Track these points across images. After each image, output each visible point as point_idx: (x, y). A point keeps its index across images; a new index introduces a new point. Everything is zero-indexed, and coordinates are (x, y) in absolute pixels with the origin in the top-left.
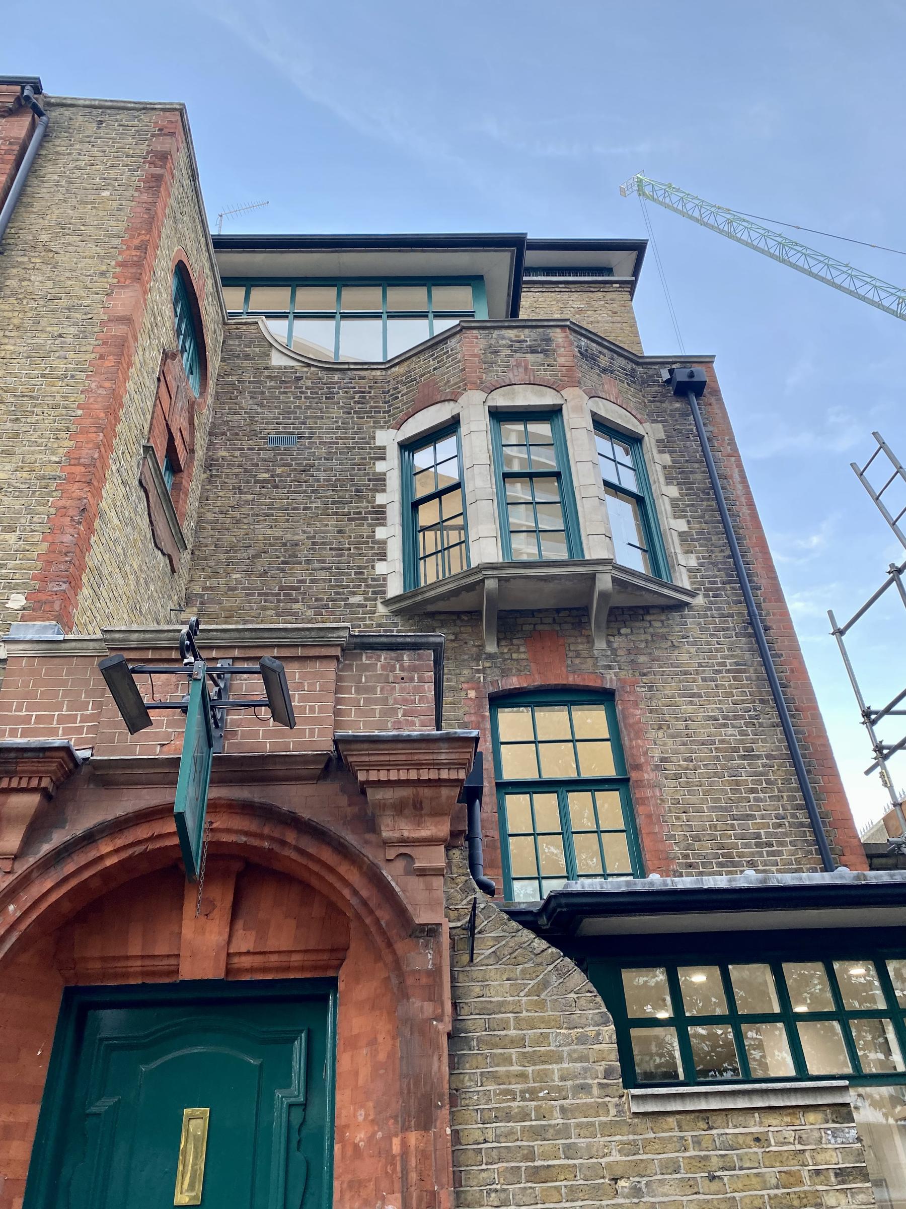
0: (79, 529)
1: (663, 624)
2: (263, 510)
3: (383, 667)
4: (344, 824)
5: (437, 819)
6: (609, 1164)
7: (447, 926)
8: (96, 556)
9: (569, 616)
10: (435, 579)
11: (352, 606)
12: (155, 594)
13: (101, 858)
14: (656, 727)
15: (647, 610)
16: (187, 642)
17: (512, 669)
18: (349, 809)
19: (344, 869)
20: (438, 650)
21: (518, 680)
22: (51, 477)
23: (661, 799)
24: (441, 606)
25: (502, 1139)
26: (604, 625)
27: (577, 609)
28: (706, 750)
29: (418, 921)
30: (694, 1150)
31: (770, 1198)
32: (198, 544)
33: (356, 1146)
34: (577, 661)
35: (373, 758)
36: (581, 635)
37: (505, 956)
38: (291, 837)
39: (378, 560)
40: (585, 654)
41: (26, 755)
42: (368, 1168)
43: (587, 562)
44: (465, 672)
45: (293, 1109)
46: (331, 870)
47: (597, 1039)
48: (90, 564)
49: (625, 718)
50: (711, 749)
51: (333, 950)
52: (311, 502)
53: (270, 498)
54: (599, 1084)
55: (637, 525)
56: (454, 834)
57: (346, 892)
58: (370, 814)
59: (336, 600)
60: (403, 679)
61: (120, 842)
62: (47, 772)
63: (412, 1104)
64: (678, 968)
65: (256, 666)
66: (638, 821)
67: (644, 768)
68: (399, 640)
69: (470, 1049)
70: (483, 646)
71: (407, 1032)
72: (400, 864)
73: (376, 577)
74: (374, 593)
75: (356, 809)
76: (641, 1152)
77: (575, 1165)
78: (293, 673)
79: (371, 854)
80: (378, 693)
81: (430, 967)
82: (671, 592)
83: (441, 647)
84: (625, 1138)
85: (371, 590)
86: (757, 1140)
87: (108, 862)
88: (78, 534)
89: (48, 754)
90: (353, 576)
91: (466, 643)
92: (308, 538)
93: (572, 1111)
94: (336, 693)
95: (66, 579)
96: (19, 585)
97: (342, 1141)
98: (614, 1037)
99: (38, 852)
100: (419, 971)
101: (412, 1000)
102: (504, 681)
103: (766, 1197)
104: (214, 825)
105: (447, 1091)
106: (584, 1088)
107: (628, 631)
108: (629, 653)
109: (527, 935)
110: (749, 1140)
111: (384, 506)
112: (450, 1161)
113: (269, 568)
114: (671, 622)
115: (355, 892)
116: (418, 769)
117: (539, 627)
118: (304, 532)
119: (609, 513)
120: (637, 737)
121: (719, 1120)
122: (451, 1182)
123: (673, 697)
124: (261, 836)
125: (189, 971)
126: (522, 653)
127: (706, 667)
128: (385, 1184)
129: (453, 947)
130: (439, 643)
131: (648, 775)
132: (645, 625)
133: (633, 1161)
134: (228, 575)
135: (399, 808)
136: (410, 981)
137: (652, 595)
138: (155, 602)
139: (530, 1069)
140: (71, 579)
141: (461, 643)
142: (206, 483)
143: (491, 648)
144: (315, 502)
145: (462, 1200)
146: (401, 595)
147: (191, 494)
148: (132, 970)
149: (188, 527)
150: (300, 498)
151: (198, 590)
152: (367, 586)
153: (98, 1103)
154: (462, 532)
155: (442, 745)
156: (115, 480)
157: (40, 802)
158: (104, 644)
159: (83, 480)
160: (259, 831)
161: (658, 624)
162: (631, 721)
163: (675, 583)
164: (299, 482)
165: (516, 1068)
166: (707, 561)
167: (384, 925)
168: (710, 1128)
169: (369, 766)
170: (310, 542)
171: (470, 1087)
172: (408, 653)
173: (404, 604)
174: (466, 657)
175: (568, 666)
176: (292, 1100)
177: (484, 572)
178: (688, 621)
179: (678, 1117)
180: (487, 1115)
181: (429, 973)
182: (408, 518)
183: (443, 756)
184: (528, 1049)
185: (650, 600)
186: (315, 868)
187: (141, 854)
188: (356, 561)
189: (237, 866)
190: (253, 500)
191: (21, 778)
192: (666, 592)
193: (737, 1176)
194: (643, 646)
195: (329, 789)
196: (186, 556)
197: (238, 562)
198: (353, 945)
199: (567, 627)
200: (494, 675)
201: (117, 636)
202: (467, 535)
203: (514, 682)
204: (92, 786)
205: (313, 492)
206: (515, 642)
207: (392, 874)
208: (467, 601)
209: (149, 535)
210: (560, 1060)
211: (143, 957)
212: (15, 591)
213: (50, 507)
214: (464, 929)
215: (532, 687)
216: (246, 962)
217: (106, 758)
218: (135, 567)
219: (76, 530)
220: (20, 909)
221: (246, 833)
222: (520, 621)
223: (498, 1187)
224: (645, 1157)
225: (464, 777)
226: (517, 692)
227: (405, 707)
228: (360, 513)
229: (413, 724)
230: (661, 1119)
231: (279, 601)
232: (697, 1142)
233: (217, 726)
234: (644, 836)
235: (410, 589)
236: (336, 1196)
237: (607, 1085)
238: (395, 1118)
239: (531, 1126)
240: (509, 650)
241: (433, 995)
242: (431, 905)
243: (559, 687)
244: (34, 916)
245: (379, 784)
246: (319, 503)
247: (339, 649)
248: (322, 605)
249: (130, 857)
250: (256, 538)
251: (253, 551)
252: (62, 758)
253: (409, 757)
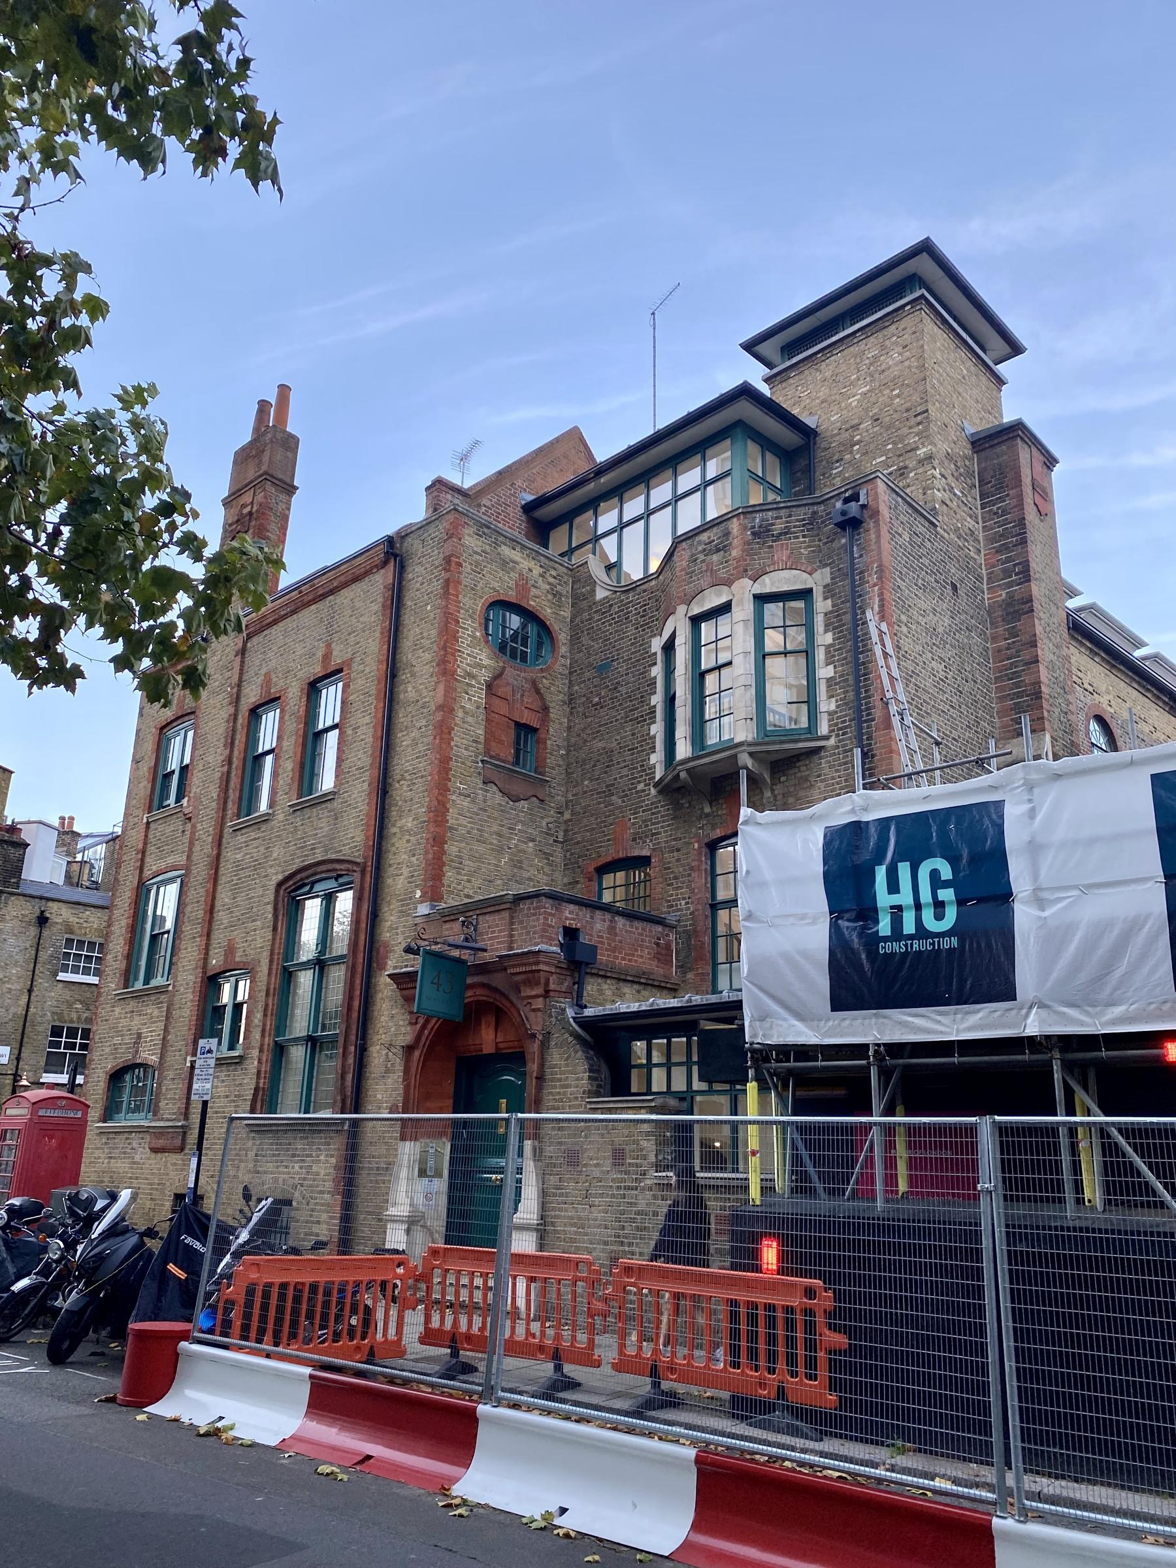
70: (703, 808)
106: (576, 1098)
143: (707, 810)
166: (843, 704)
178: (823, 761)
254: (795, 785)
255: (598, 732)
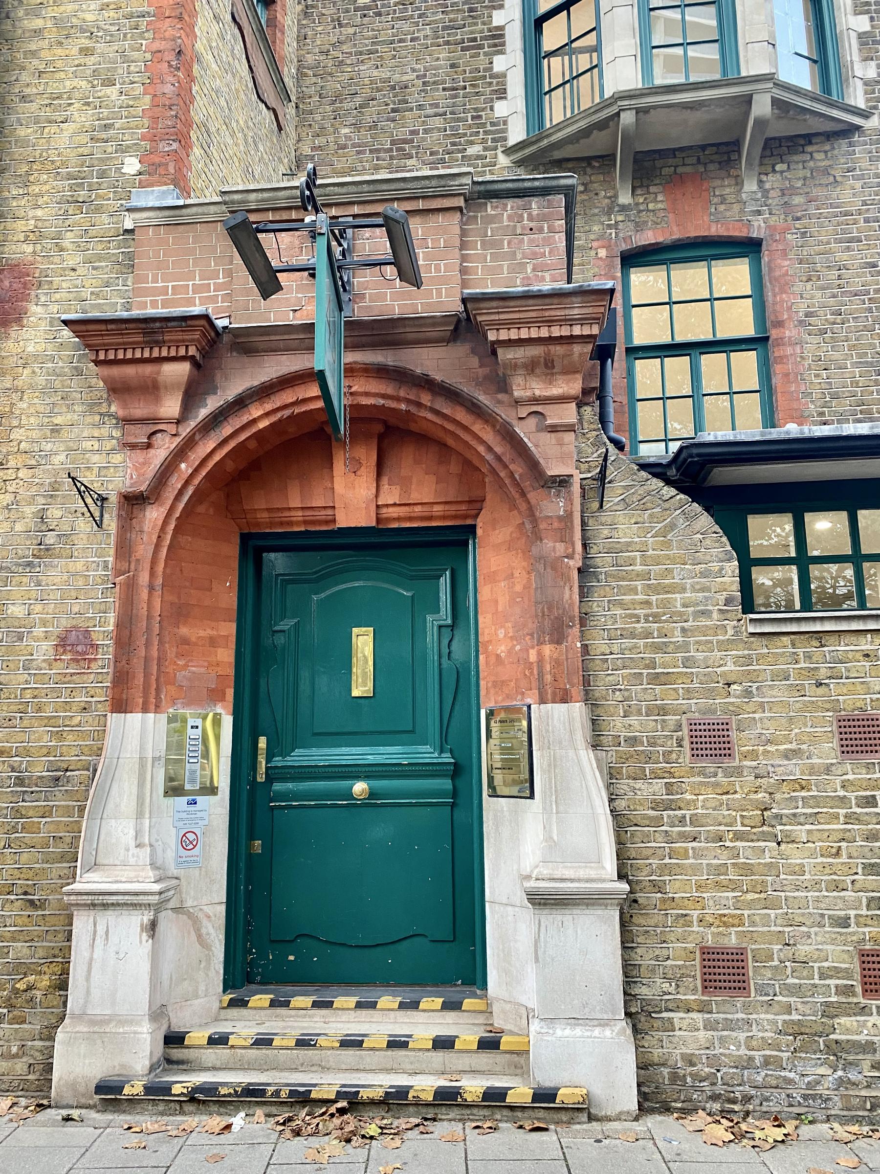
0: (179, 76)
1: (826, 156)
2: (367, 46)
3: (510, 218)
4: (476, 385)
5: (570, 377)
6: (724, 672)
7: (577, 477)
8: (200, 110)
9: (716, 153)
10: (562, 119)
11: (469, 158)
12: (265, 156)
13: (254, 421)
14: (804, 279)
15: (809, 138)
16: (307, 193)
17: (647, 222)
18: (480, 370)
19: (478, 427)
20: (569, 193)
21: (654, 235)
22: (139, 14)
23: (801, 357)
24: (568, 152)
25: (626, 652)
26: (757, 162)
27: (727, 144)
28: (858, 302)
29: (550, 473)
30: (804, 662)
31: (872, 700)
32: (301, 95)
33: (498, 656)
34: (722, 208)
35: (502, 317)
36: (729, 176)
37: (633, 502)
38: (426, 399)
39: (497, 98)
40: (731, 199)
41: (169, 324)
42: (508, 672)
43: (743, 80)
44: (595, 228)
45: (443, 630)
46: (466, 428)
47: (720, 573)
48: (196, 118)
49: (771, 270)
50: (864, 300)
51: (470, 502)
52: (418, 30)
53: (373, 30)
54: (720, 610)
55: (808, 28)
56: (586, 392)
57: (481, 449)
58: (501, 375)
59: (452, 153)
60: (531, 229)
61: (268, 407)
62: (192, 340)
63: (546, 624)
64: (805, 514)
65: (380, 221)
66: (774, 381)
67: (787, 325)
68: (528, 184)
69: (598, 581)
70: (616, 196)
71: (541, 567)
72: (532, 422)
73: (495, 120)
74: (494, 140)
75: (487, 370)
76: (755, 663)
77: (692, 673)
78: (417, 228)
79: (505, 413)
80: (506, 247)
81: (561, 513)
82: (841, 113)
83: (573, 190)
84: (740, 653)
85: (490, 137)
86: (867, 656)
87: (262, 425)
88: (178, 82)
89: (190, 323)
90: (470, 122)
91: (597, 194)
92: (417, 76)
93: (691, 631)
94: (461, 250)
95: (175, 137)
96: (130, 147)
97: (486, 651)
98: (737, 571)
99: (197, 417)
100: (551, 517)
101: (545, 541)
102: (638, 236)
103: (869, 700)
104: (353, 390)
105: (577, 614)
107: (784, 167)
108: (783, 195)
109: (656, 483)
110: (859, 656)
111: (501, 28)
112: (581, 667)
113: (378, 118)
114: (836, 152)
115: (490, 449)
116: (549, 326)
117: (680, 170)
118: (414, 70)
119: (776, 11)
120: (783, 291)
121: (832, 639)
122: (581, 682)
123: (828, 243)
124: (398, 399)
125: (343, 522)
126: (659, 202)
127: (871, 205)
128: (524, 683)
129: (583, 496)
130: (570, 186)
131: (789, 332)
132: (804, 159)
133: (746, 670)
134: (336, 131)
135: (531, 367)
136: (543, 526)
137: (817, 118)
138: (266, 164)
139: (654, 598)
140: (180, 137)
141: (592, 194)
142: (302, 17)
143: (625, 198)
144: (423, 29)
145: (590, 696)
146: (524, 141)
147: (287, 32)
148: (295, 519)
149: (289, 73)
150: (406, 26)
151: (307, 150)
152: (486, 133)
153: (281, 623)
154: (595, 55)
155: (574, 299)
156: (207, 14)
157: (191, 370)
158: (224, 208)
159: (173, 15)
160: (395, 394)
161: (821, 156)
162: (777, 273)
163: (847, 101)
164: (404, 4)
165: (641, 597)
167: (518, 477)
168: (822, 646)
169: (499, 325)
170: (420, 82)
171: (598, 611)
172: (536, 199)
173: (527, 151)
174: (596, 211)
175: (711, 214)
176: (442, 623)
177: (619, 103)
178: (857, 149)
179: (793, 637)
180: (613, 634)
181: (560, 518)
182: (530, 38)
183: (576, 311)
184: (652, 582)
185: (816, 125)
186: (450, 427)
187: (289, 417)
188: (473, 102)
189: (379, 428)
190: (355, 34)
191: (169, 347)
192: (836, 113)
193: (843, 684)
194: (799, 184)
195: (459, 351)
196: (291, 110)
197: (345, 114)
198: (488, 498)
199: (711, 167)
200: (626, 230)
201: (236, 197)
202: (600, 58)
203: (648, 237)
204: (235, 354)
205: (420, 16)
206: (652, 189)
207: (524, 431)
208: (598, 143)
209: (251, 85)
210: (684, 590)
211: (302, 508)
212: (127, 154)
213: (145, 52)
214: (594, 480)
215: (669, 242)
216: (393, 512)
217: (243, 325)
218: (241, 123)
219: (176, 78)
220: (191, 467)
221: (384, 396)
222: (659, 163)
223: (622, 687)
224: (757, 667)
225: (598, 333)
226: (652, 248)
227: (534, 261)
228: (474, 40)
229: (543, 279)
230: (775, 638)
231: (391, 158)
232: (808, 657)
233: (345, 290)
234: (779, 394)
235: (534, 131)
236: (482, 693)
237: (727, 611)
238: (532, 635)
239: (653, 642)
240: (646, 199)
241: (564, 535)
242: (563, 458)
243: (700, 240)
244: (204, 473)
245: (510, 343)
246: (428, 30)
247: (462, 198)
248: (438, 159)
249: (280, 421)
250: (361, 83)
251: (360, 99)
252: (203, 326)
253: (540, 314)
254: (805, 179)
255: (370, 52)
